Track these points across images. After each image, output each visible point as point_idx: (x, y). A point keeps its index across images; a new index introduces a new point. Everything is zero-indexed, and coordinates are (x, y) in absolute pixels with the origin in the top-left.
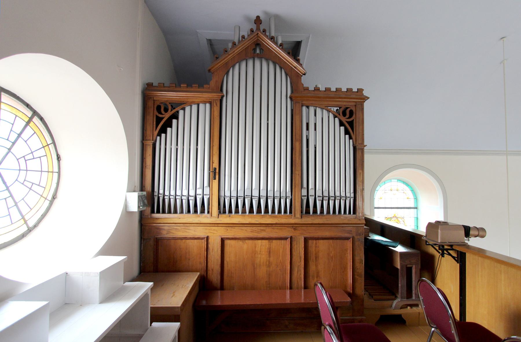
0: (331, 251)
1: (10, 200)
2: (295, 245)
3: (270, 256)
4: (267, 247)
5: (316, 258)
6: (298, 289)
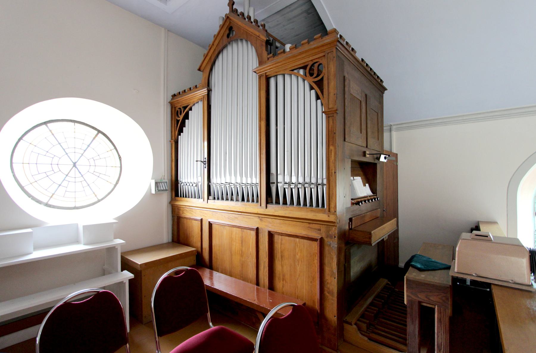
0: (297, 253)
1: (84, 182)
2: (261, 238)
3: (242, 246)
4: (240, 236)
5: (282, 257)
6: (264, 288)
